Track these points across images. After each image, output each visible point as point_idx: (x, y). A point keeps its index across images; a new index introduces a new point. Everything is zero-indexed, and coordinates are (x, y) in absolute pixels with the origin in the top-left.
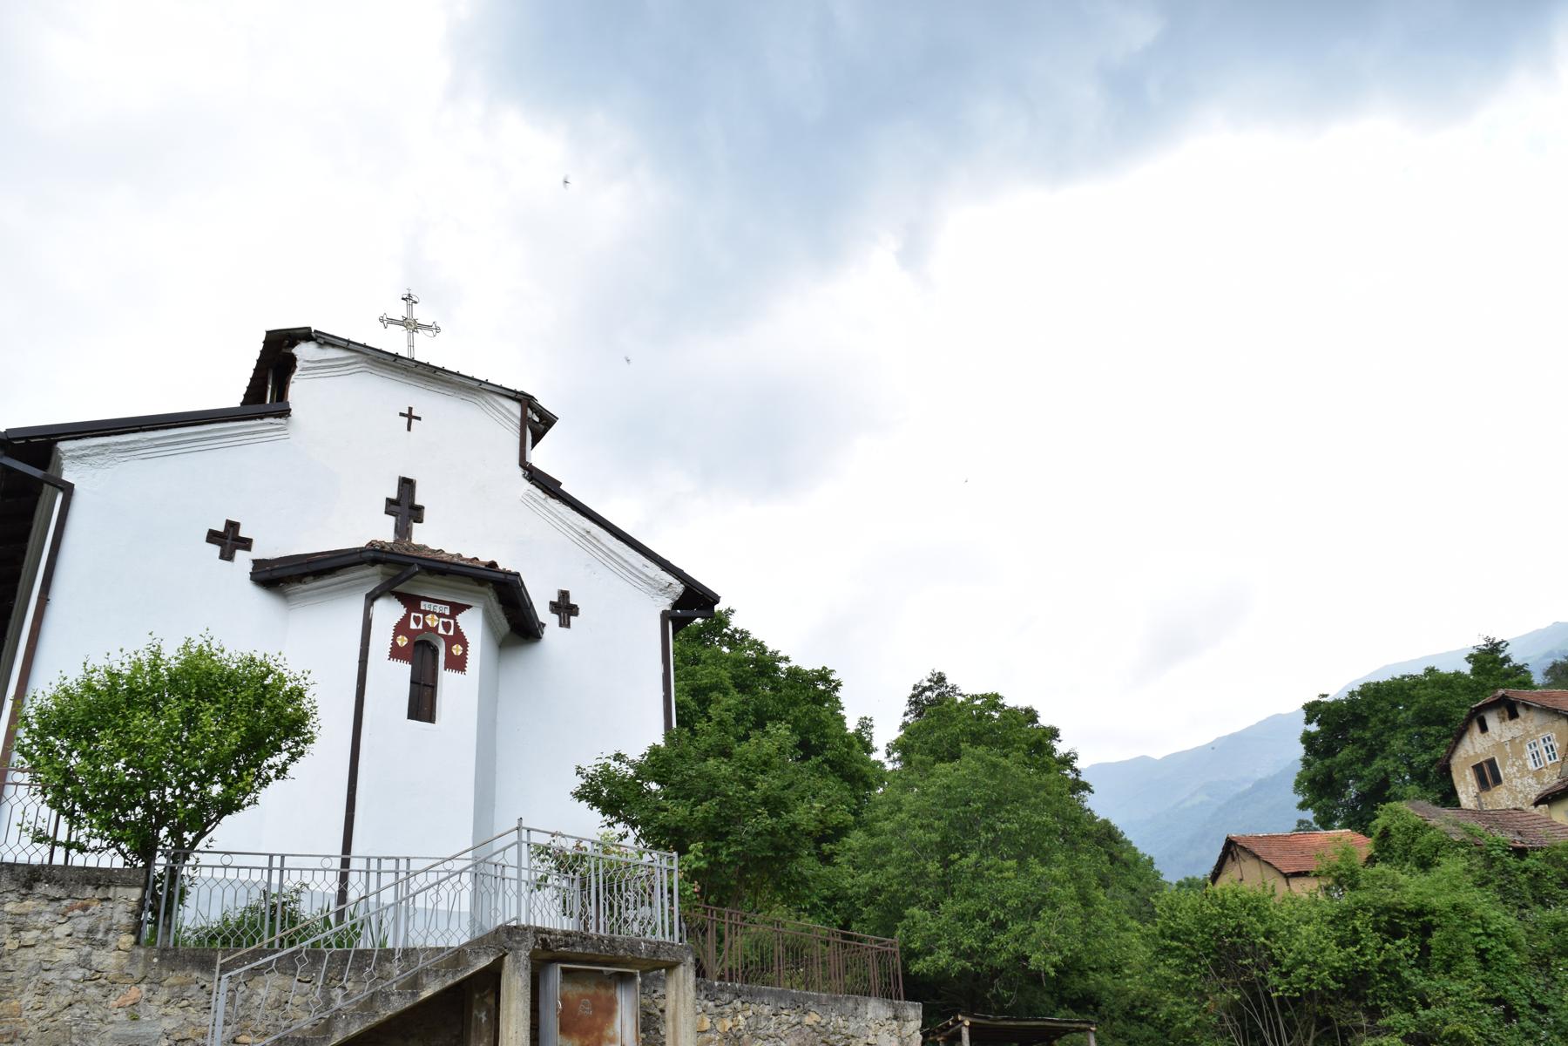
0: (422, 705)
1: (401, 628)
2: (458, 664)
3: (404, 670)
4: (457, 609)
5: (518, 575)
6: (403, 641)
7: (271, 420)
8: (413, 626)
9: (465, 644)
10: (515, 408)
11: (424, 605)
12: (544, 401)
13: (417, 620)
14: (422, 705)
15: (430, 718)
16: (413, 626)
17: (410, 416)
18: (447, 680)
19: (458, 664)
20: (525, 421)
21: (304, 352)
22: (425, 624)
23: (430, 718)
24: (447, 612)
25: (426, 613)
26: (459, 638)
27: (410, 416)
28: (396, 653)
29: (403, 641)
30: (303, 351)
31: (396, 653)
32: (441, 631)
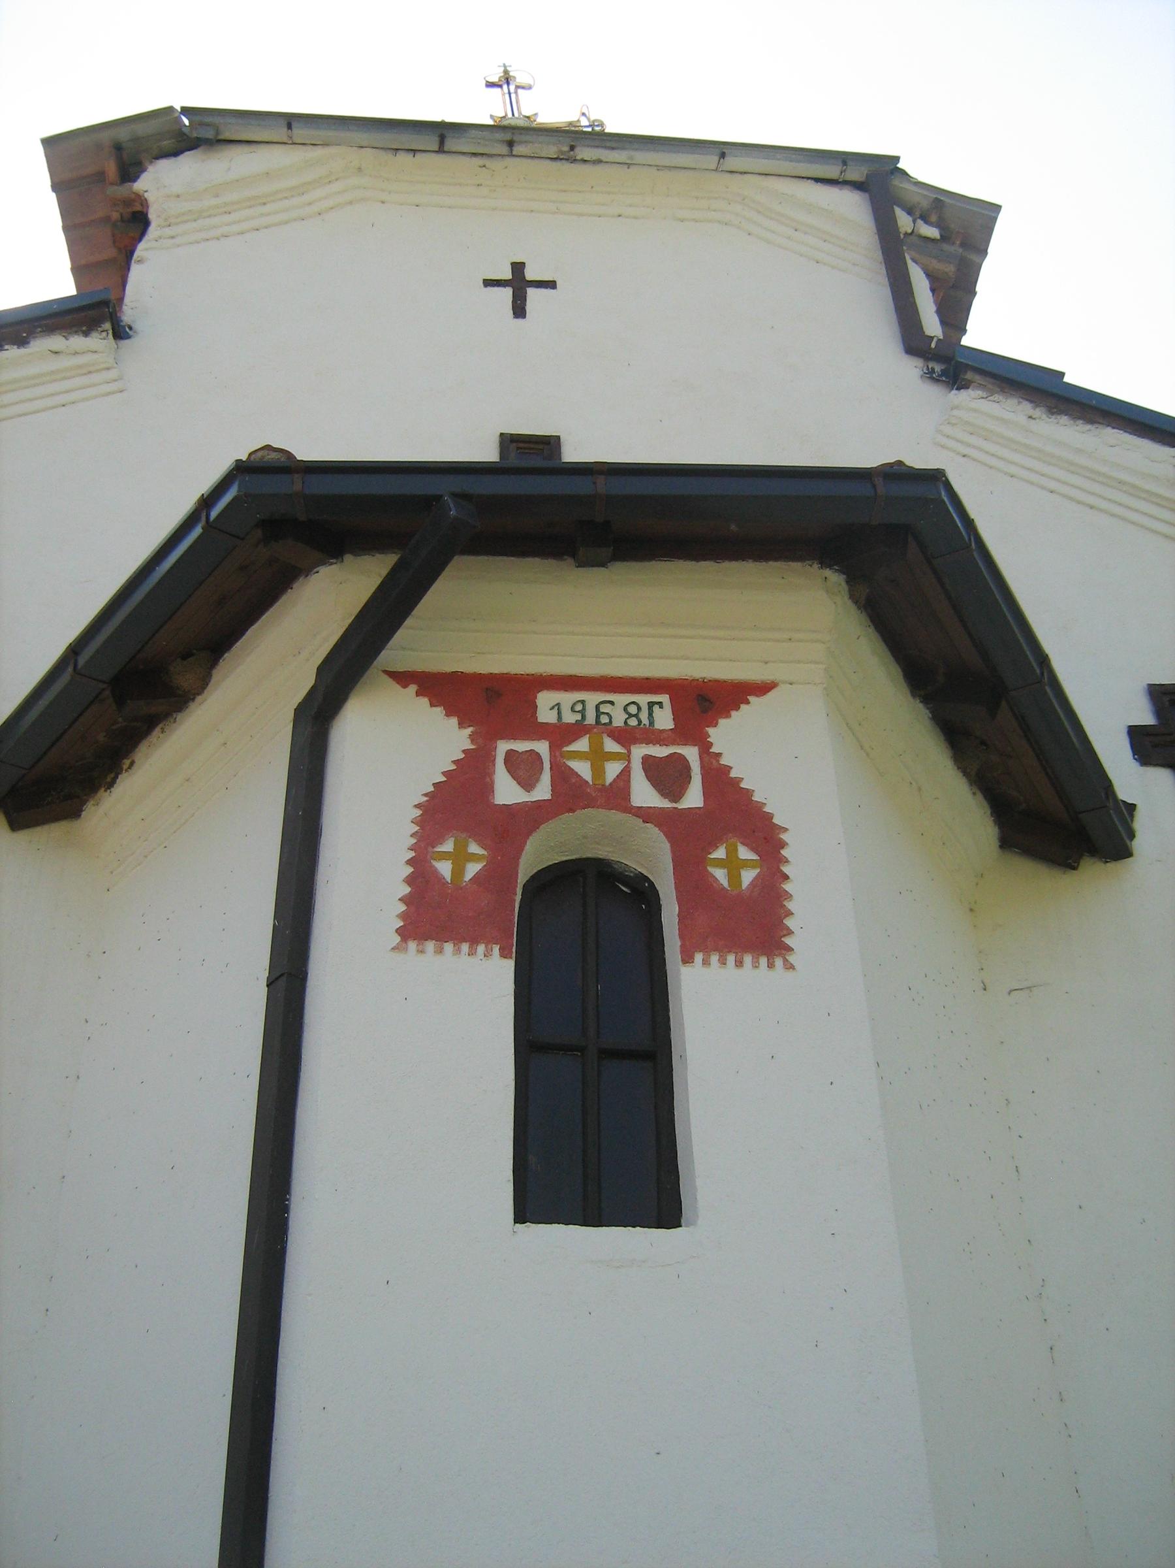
0: (597, 1134)
1: (455, 803)
2: (757, 926)
3: (480, 988)
4: (703, 703)
5: (936, 477)
6: (463, 862)
7: (56, 342)
8: (507, 791)
9: (767, 838)
10: (851, 206)
11: (549, 706)
12: (927, 166)
13: (524, 769)
14: (597, 1134)
15: (656, 1199)
16: (507, 791)
17: (518, 284)
18: (712, 1003)
19: (757, 926)
20: (893, 249)
21: (161, 183)
22: (562, 776)
23: (656, 1199)
24: (664, 720)
25: (560, 735)
26: (736, 813)
27: (518, 284)
28: (431, 915)
29: (463, 862)
30: (161, 183)
31: (431, 915)
32: (644, 794)
